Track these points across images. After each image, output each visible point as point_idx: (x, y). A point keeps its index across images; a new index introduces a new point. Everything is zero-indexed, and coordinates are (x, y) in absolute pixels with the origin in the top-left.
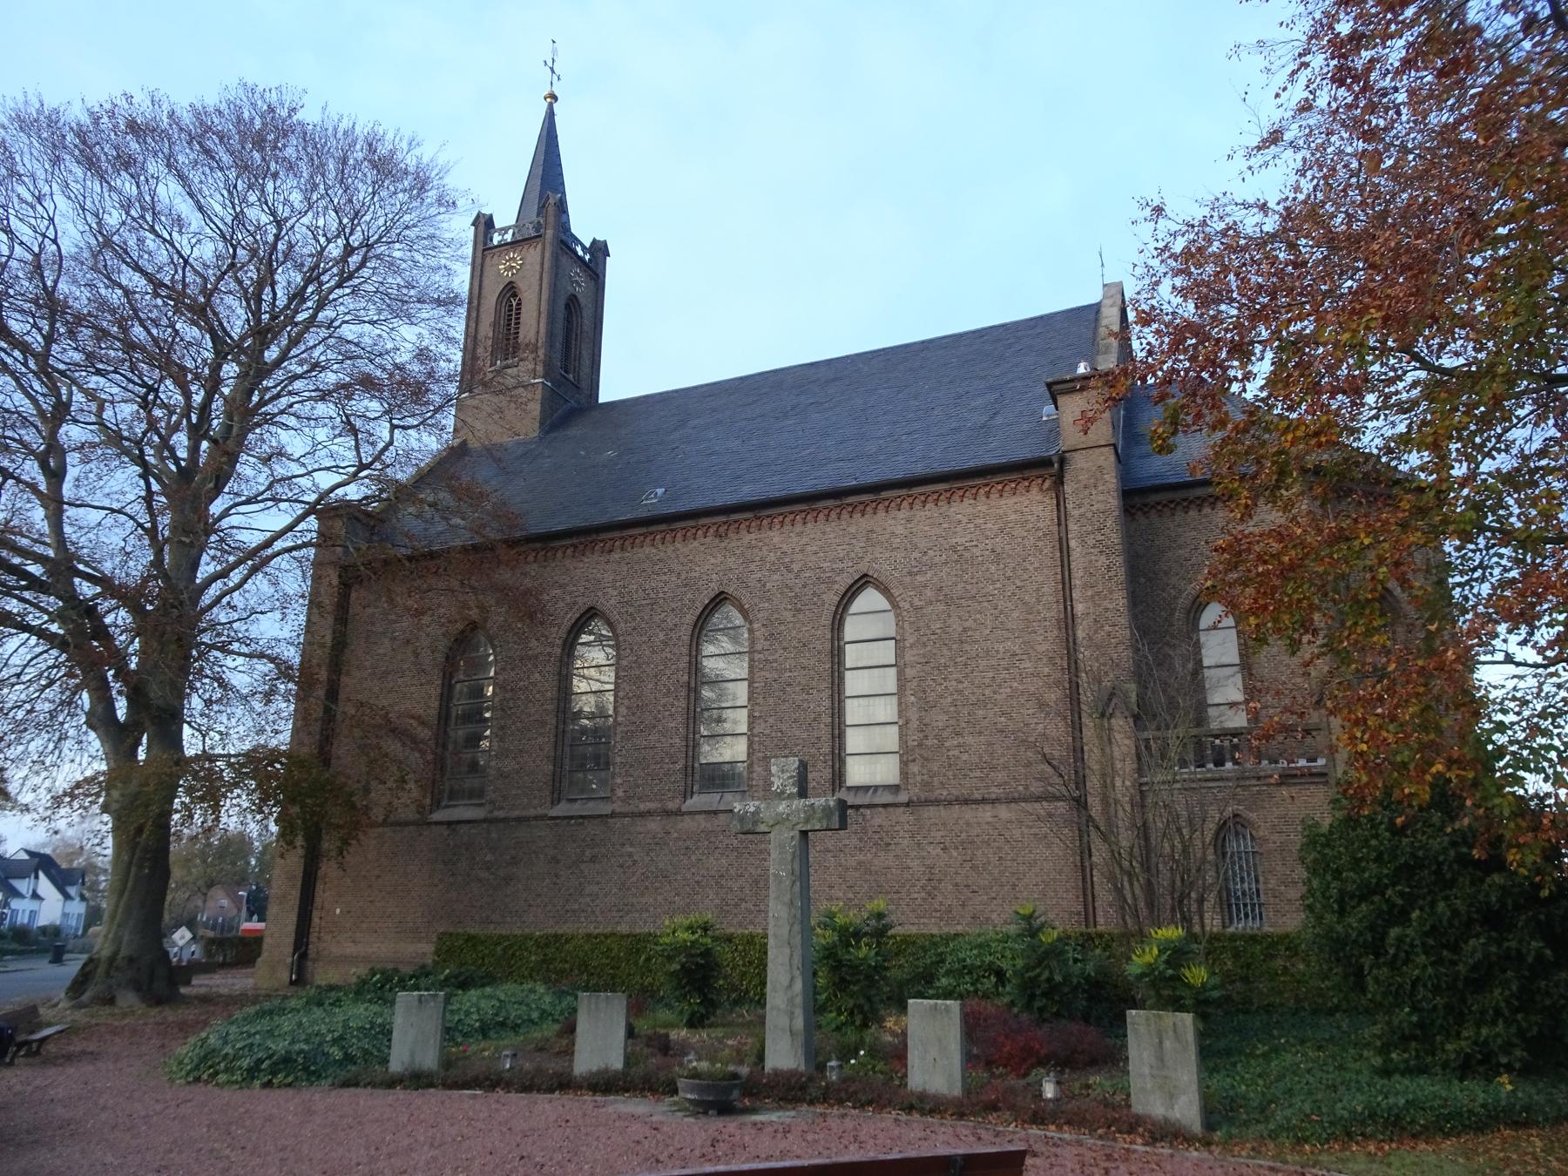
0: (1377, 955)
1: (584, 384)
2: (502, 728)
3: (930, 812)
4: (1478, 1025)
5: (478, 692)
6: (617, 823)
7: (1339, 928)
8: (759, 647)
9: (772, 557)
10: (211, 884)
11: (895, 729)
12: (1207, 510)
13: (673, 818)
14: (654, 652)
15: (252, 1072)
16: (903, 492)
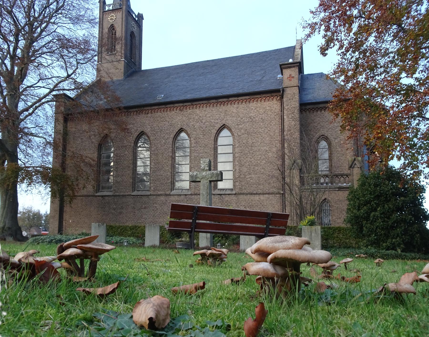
0: (367, 221)
1: (137, 64)
2: (117, 168)
3: (241, 197)
4: (392, 239)
5: (109, 157)
6: (152, 198)
7: (358, 213)
8: (193, 146)
9: (197, 118)
10: (31, 227)
11: (232, 172)
12: (323, 112)
13: (168, 196)
14: (161, 146)
15: (50, 242)
16: (236, 98)
